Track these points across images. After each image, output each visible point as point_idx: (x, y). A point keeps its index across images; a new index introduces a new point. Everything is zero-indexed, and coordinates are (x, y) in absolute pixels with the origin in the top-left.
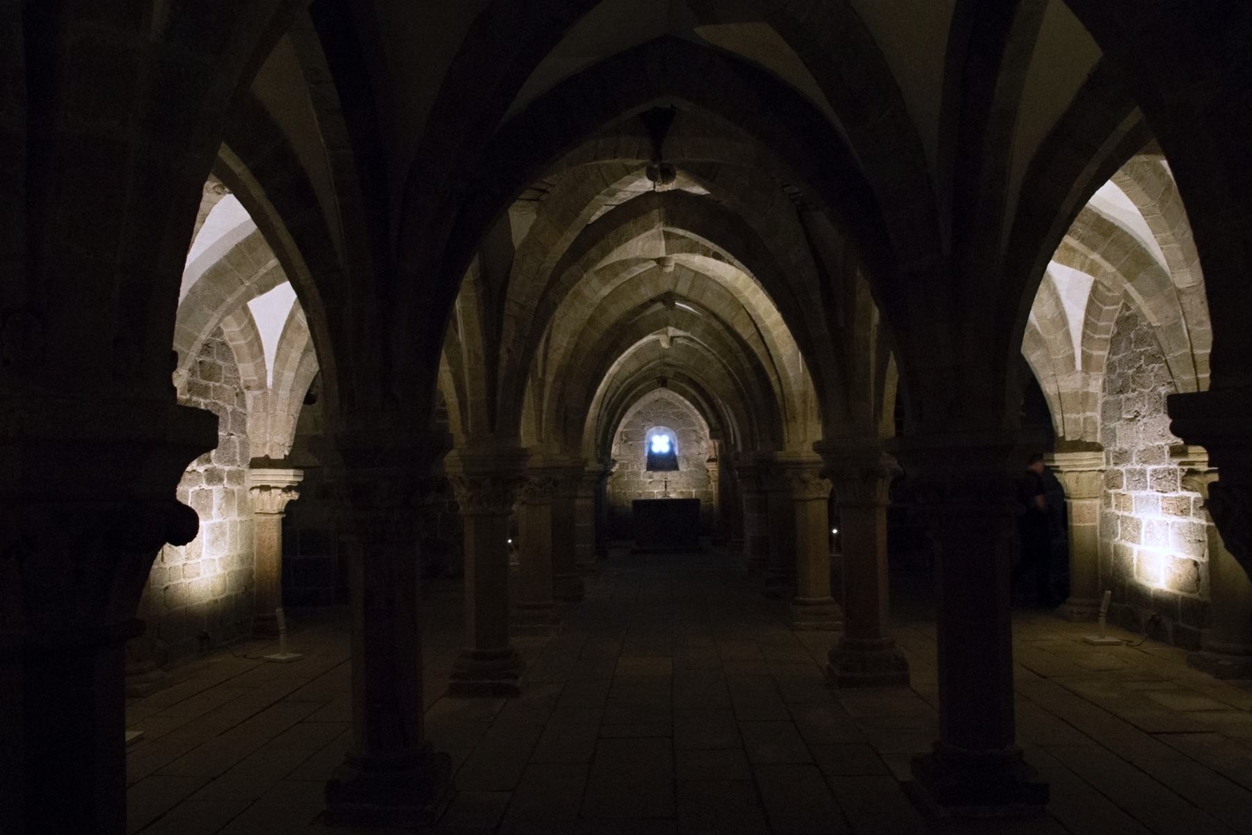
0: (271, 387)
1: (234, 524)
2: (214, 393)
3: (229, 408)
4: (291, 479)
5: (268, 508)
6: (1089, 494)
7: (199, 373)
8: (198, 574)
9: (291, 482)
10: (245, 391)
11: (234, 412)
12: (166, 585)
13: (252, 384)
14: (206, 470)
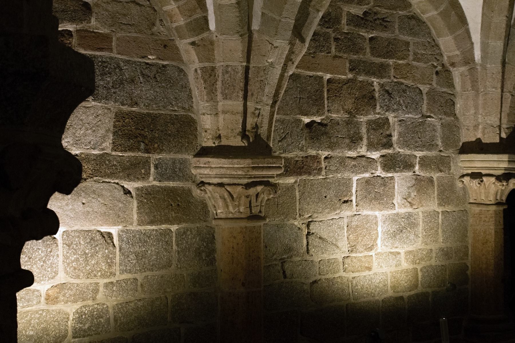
0: (480, 62)
1: (432, 216)
2: (395, 72)
3: (424, 88)
4: (505, 165)
5: (482, 198)
6: (262, 116)
7: (368, 50)
8: (369, 269)
9: (506, 169)
10: (451, 69)
11: (431, 93)
12: (314, 279)
13: (456, 60)
14: (382, 156)
